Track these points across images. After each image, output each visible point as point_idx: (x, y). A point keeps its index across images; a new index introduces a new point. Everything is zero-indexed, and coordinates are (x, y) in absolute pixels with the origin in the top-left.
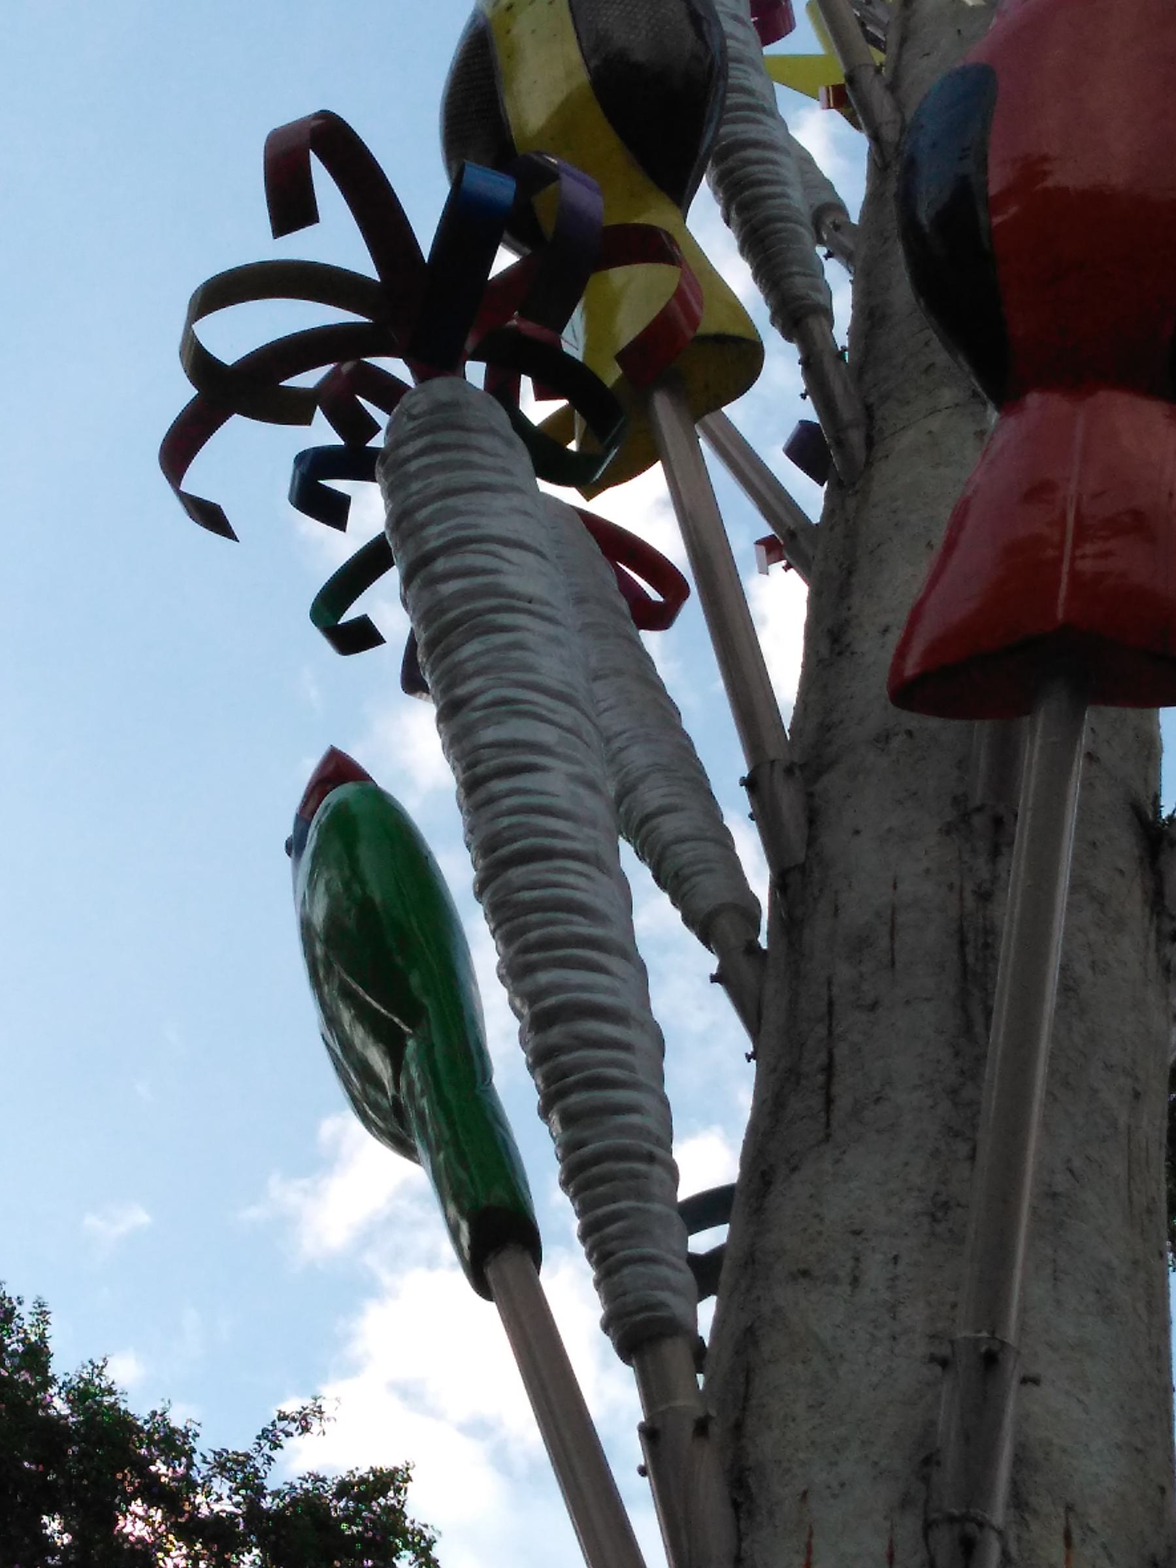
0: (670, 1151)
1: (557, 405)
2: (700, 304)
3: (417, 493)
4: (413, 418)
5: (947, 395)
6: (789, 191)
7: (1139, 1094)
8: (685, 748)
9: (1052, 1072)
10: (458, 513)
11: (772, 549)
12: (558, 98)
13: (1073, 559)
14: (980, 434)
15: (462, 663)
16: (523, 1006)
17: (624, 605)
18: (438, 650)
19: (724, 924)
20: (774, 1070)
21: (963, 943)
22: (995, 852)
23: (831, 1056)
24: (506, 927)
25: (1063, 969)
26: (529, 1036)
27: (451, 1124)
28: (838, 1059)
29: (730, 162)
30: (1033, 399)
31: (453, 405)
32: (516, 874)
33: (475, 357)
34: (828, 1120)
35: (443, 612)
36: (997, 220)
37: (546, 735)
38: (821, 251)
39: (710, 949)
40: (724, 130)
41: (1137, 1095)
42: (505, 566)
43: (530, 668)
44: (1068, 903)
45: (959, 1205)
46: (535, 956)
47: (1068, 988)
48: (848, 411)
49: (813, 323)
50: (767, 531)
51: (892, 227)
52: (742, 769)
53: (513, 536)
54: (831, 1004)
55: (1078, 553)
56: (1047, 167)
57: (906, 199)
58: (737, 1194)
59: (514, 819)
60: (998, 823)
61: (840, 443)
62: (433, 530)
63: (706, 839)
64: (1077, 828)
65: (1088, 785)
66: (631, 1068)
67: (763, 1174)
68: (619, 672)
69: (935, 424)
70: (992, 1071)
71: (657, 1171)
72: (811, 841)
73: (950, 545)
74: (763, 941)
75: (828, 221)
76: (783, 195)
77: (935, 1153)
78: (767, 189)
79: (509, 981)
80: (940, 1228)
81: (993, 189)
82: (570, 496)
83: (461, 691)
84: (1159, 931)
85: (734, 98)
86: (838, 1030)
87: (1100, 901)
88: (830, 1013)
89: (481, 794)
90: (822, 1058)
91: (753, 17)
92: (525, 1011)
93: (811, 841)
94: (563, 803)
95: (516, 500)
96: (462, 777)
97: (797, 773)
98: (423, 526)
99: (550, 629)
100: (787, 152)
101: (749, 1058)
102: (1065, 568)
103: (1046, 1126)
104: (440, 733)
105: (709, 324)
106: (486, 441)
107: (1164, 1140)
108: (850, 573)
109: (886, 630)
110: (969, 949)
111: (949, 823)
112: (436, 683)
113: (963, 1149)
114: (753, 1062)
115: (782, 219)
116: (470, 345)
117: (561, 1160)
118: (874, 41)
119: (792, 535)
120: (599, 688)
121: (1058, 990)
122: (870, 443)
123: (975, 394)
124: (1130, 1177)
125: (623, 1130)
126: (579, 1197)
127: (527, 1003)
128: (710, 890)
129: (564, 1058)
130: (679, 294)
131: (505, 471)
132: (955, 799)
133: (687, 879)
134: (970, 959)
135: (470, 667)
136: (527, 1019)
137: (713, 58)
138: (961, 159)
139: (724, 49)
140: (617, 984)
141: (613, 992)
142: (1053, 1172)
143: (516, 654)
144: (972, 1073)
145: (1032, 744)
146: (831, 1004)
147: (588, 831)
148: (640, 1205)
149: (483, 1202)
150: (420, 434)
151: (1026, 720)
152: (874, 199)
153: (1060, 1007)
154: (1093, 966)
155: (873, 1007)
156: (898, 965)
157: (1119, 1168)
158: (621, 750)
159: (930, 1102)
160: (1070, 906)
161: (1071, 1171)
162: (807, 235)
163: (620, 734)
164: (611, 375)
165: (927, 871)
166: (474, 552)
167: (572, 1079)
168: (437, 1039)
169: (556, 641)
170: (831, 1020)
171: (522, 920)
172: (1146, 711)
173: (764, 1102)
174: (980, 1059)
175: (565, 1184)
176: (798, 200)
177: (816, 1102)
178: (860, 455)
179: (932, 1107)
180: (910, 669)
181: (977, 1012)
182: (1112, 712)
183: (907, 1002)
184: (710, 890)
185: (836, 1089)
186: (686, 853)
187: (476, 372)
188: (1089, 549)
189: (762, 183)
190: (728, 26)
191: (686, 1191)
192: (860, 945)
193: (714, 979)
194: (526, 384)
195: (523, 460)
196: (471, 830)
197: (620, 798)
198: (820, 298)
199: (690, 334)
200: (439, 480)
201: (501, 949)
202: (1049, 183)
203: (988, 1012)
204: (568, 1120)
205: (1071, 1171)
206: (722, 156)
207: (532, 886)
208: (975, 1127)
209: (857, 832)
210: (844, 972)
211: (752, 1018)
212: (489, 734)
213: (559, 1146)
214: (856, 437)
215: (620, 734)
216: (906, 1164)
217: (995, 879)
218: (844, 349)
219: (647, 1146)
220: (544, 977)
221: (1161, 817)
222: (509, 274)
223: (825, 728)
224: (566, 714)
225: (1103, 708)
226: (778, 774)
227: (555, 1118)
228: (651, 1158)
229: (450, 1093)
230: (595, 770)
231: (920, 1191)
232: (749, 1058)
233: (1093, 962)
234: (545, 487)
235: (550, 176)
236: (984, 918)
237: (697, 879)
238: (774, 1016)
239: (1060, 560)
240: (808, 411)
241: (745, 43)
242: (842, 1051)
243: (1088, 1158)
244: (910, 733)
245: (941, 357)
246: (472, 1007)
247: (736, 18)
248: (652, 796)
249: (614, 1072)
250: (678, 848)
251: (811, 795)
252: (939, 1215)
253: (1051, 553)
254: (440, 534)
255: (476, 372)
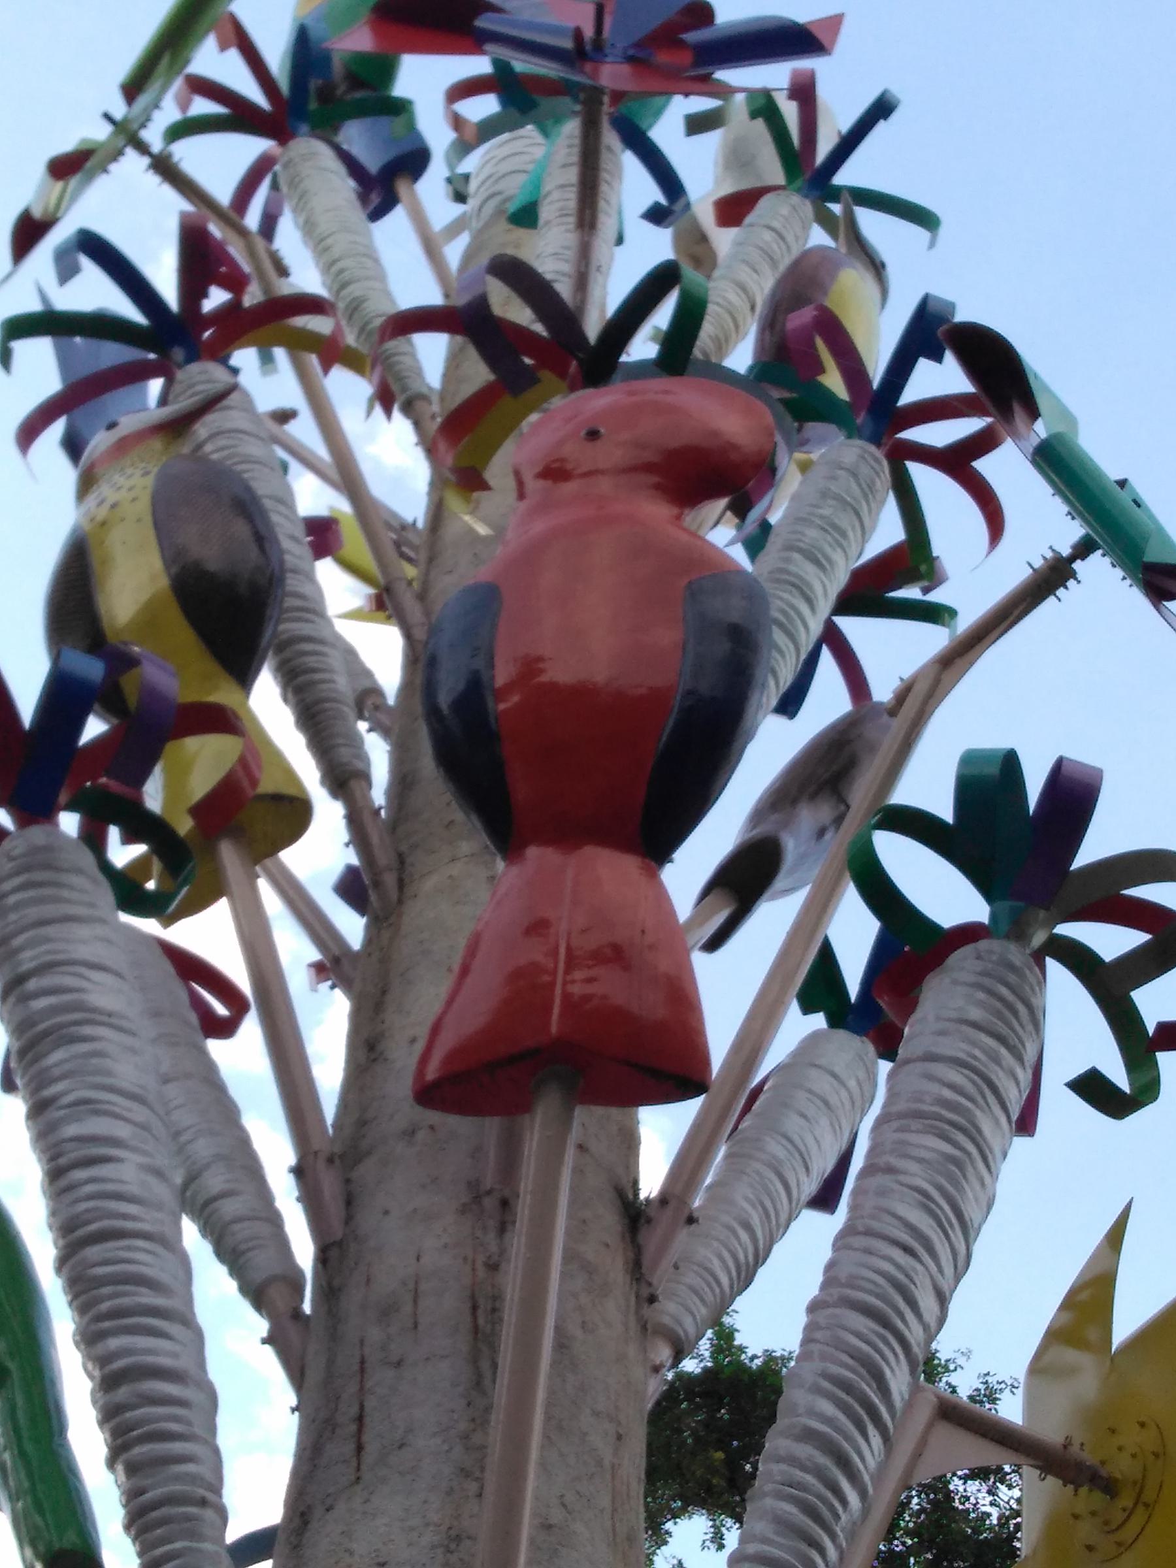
0: (220, 1496)
1: (139, 849)
2: (259, 767)
3: (16, 922)
4: (11, 859)
5: (465, 847)
6: (336, 677)
7: (621, 1435)
8: (243, 1142)
9: (548, 1418)
10: (48, 940)
11: (320, 970)
12: (144, 597)
13: (565, 984)
14: (492, 878)
15: (48, 1068)
16: (94, 1369)
17: (193, 1018)
18: (30, 1056)
19: (277, 1294)
20: (314, 1421)
21: (475, 1308)
22: (503, 1228)
23: (362, 1407)
24: (83, 1298)
25: (557, 1328)
26: (99, 1395)
27: (30, 1475)
28: (367, 1409)
29: (287, 653)
30: (532, 852)
31: (48, 849)
32: (93, 1252)
33: (70, 807)
34: (359, 1464)
35: (34, 1024)
36: (502, 706)
37: (122, 1131)
38: (362, 726)
39: (263, 1317)
40: (282, 627)
41: (619, 1437)
42: (85, 984)
43: (109, 1073)
44: (562, 1272)
45: (469, 1538)
46: (107, 1324)
47: (562, 1345)
48: (384, 858)
49: (354, 784)
50: (315, 955)
51: (419, 708)
52: (290, 1157)
53: (96, 960)
54: (362, 1362)
55: (569, 978)
56: (541, 665)
57: (429, 690)
58: (279, 1532)
59: (91, 1204)
60: (505, 1204)
61: (377, 884)
62: (27, 954)
63: (257, 1219)
64: (569, 1206)
65: (578, 1171)
66: (189, 1423)
67: (303, 1514)
68: (188, 1076)
69: (456, 869)
70: (498, 1417)
71: (209, 1514)
72: (349, 1219)
73: (465, 970)
74: (307, 1308)
75: (369, 702)
76: (333, 682)
77: (450, 1492)
78: (317, 676)
79: (83, 1347)
80: (453, 1558)
81: (500, 681)
82: (149, 926)
83: (48, 1092)
84: (637, 1297)
85: (290, 602)
86: (369, 1384)
87: (589, 1269)
88: (362, 1370)
89: (63, 1182)
90: (354, 1410)
91: (308, 535)
92: (97, 1373)
93: (349, 1219)
94: (134, 1189)
95: (99, 930)
96: (46, 1167)
97: (337, 1162)
98: (21, 949)
99: (128, 1040)
100: (333, 646)
101: (293, 1410)
102: (558, 991)
103: (543, 1465)
104: (28, 1128)
105: (268, 784)
106: (75, 880)
107: (643, 1476)
108: (384, 992)
109: (413, 1041)
110: (480, 1312)
111: (464, 1205)
112: (26, 1085)
113: (473, 1487)
114: (297, 1413)
115: (327, 700)
116: (63, 798)
117: (125, 1506)
118: (410, 560)
119: (336, 961)
120: (172, 1091)
121: (553, 1347)
122: (401, 884)
123: (487, 847)
124: (614, 1510)
125: (178, 1478)
126: (139, 1539)
127: (98, 1366)
128: (263, 1263)
129: (128, 1415)
130: (243, 762)
131: (92, 905)
132: (469, 1183)
133: (243, 1253)
134: (481, 1321)
135: (56, 1072)
136: (98, 1379)
137: (273, 570)
138: (473, 657)
139: (282, 562)
140: (177, 1348)
141: (175, 1355)
142: (548, 1506)
143: (94, 1061)
144: (480, 1420)
145: (532, 1140)
146: (362, 1362)
147: (159, 1215)
148: (195, 1545)
149: (57, 1546)
150: (17, 873)
151: (527, 1116)
152: (406, 687)
153: (554, 1364)
154: (584, 1324)
155: (399, 1364)
156: (420, 1328)
157: (605, 1501)
158: (190, 1142)
159: (446, 1447)
160: (564, 1275)
161: (564, 1505)
162: (349, 711)
163: (188, 1128)
164: (184, 825)
165: (446, 1246)
166: (63, 973)
167: (135, 1433)
168: (20, 1401)
169: (133, 1051)
170: (362, 1377)
171: (95, 1292)
172: (627, 1110)
173: (305, 1449)
174: (488, 1409)
175: (128, 1527)
176: (342, 684)
177: (350, 1447)
178: (393, 894)
179: (447, 1451)
180: (431, 1074)
181: (485, 1365)
182: (599, 1111)
183: (428, 1359)
184: (263, 1263)
185: (365, 1438)
186: (242, 1231)
187: (69, 822)
188: (578, 975)
189: (314, 670)
190: (286, 544)
191: (233, 1534)
192: (386, 1312)
193: (265, 1341)
194: (114, 833)
195: (105, 895)
196: (53, 1213)
197: (186, 1185)
198: (360, 765)
199: (251, 793)
200: (33, 913)
201: (77, 1319)
202: (544, 678)
203: (495, 1366)
204: (132, 1470)
205: (564, 1505)
206: (281, 648)
207: (106, 1262)
208: (482, 1469)
209: (386, 1212)
210: (375, 1334)
211: (297, 1374)
212: (71, 1130)
213: (123, 1493)
214: (390, 879)
215: (188, 1128)
216: (425, 1502)
217: (503, 1252)
218: (380, 808)
219: (201, 1492)
220: (114, 1343)
221: (639, 1198)
222: (99, 743)
223: (362, 1123)
224: (139, 1113)
225: (593, 1108)
226: (321, 1165)
227: (120, 1468)
228: (203, 1503)
229: (29, 1447)
230: (162, 1160)
231: (437, 1525)
232: (293, 1410)
233: (583, 1322)
234: (125, 918)
235: (131, 662)
236: (493, 1286)
237: (250, 1254)
238: (314, 1375)
239: (553, 984)
240: (352, 858)
241: (300, 557)
242: (370, 1403)
243: (578, 1493)
244: (432, 1127)
245: (459, 815)
246: (51, 1370)
247: (293, 538)
248: (214, 1181)
249: (174, 1427)
250: (236, 1227)
251: (348, 1181)
252: (453, 1546)
253: (546, 978)
254: (32, 959)
255: (69, 822)
